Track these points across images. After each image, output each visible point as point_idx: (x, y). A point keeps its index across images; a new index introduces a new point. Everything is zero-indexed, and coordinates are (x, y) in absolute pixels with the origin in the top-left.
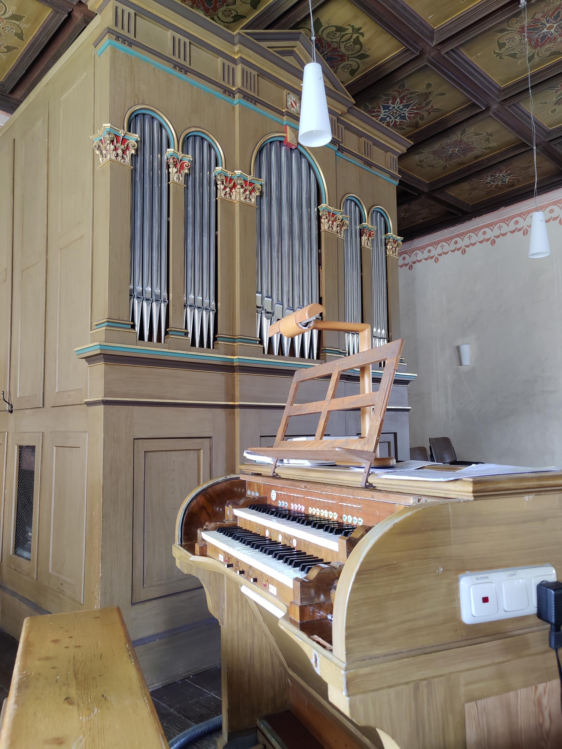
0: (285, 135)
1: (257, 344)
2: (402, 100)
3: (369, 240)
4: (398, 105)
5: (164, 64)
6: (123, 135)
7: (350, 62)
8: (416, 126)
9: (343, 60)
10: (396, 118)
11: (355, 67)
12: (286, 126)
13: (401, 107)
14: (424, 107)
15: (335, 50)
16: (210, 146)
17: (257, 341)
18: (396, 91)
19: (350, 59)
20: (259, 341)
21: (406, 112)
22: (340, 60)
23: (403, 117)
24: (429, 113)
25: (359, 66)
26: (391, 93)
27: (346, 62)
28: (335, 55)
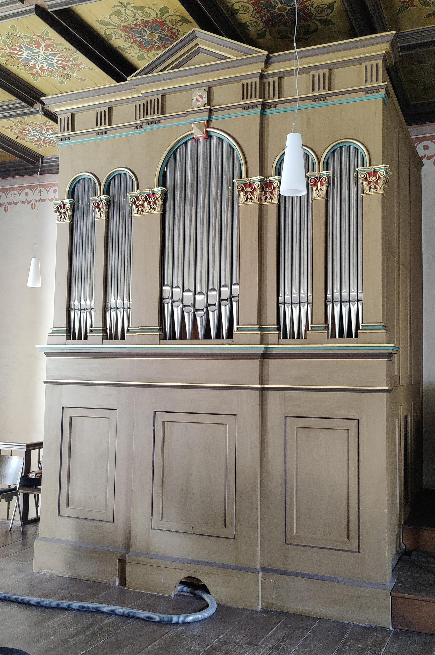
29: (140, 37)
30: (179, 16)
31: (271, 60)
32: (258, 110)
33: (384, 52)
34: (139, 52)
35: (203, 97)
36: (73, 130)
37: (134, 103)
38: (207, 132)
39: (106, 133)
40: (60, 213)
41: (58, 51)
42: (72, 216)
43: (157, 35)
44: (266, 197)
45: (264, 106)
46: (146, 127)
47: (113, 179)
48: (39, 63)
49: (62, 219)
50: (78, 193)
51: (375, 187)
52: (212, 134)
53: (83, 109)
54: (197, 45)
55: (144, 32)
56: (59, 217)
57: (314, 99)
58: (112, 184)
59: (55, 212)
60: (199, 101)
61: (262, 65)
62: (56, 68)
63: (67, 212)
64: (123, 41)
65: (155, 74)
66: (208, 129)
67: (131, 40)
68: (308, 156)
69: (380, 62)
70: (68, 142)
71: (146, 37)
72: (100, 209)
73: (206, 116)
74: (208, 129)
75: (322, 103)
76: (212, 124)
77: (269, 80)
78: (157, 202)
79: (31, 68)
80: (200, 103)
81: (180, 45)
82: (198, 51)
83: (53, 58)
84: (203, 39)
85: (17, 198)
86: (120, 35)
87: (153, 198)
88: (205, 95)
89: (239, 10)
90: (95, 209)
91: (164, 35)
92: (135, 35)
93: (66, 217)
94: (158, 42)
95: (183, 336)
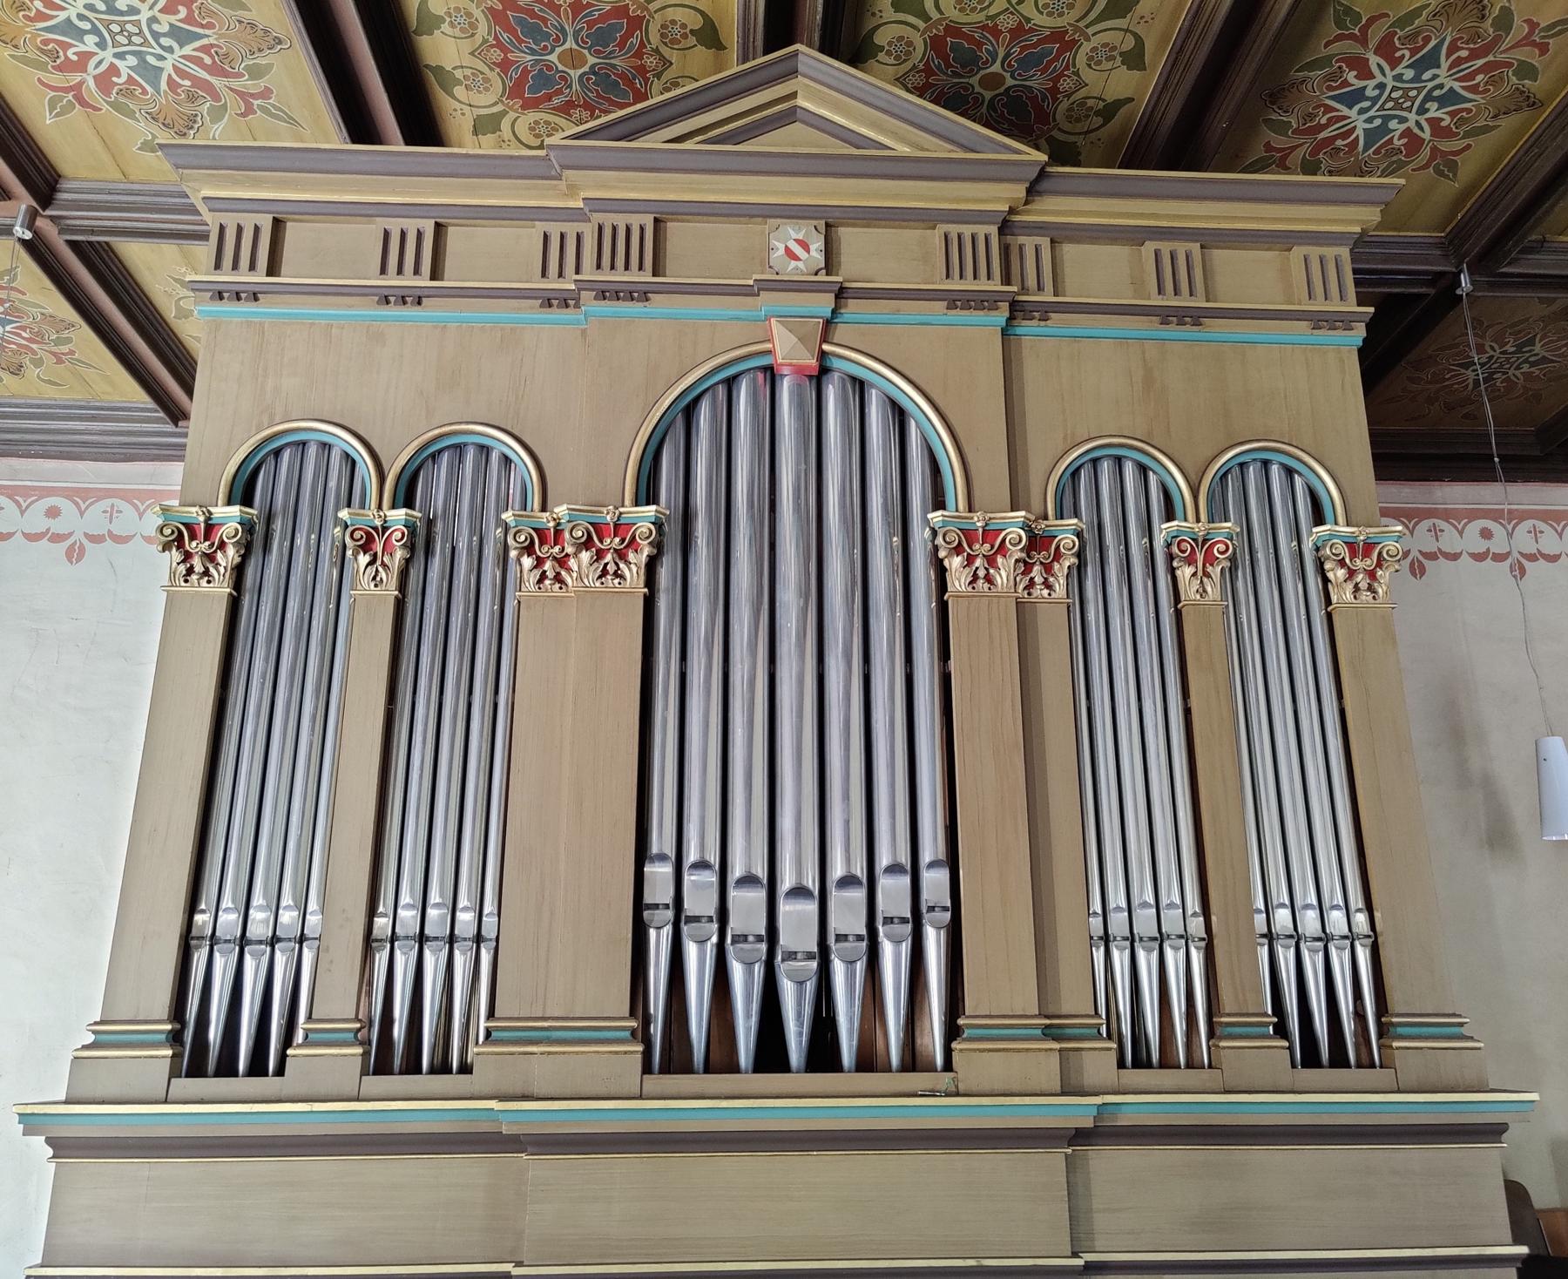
0: (769, 346)
1: (1266, 1037)
2: (1386, 50)
3: (1206, 574)
4: (1383, 74)
5: (350, 307)
6: (202, 519)
7: (1096, 41)
8: (1530, 102)
9: (1072, 45)
10: (1422, 110)
11: (1130, 43)
12: (768, 318)
13: (1409, 74)
14: (1497, 40)
15: (1018, 32)
16: (899, 415)
17: (1266, 1025)
18: (1339, 38)
19: (1090, 31)
20: (1275, 1025)
21: (1443, 76)
22: (1061, 52)
23: (1450, 98)
24: (1544, 48)
25: (1135, 35)
26: (1324, 52)
27: (1086, 47)
28: (1034, 46)
29: (533, 52)
30: (702, 13)
31: (1045, 185)
32: (1000, 317)
33: (1358, 229)
34: (496, 103)
35: (813, 247)
36: (273, 270)
37: (541, 227)
38: (823, 355)
39: (419, 303)
40: (188, 556)
41: (210, 26)
42: (239, 571)
43: (592, 60)
44: (1032, 583)
45: (1018, 310)
46: (592, 306)
47: (271, 459)
48: (108, 55)
49: (194, 577)
50: (276, 486)
51: (1370, 588)
52: (836, 363)
53: (332, 209)
54: (794, 95)
55: (557, 40)
56: (182, 569)
57: (1166, 316)
58: (267, 474)
59: (166, 547)
60: (796, 258)
61: (1019, 191)
62: (164, 86)
63: (219, 555)
64: (466, 46)
65: (653, 141)
66: (826, 347)
67: (496, 55)
68: (354, 462)
69: (1344, 252)
70: (246, 307)
71: (553, 58)
72: (375, 556)
73: (823, 304)
74: (826, 347)
75: (1188, 332)
76: (840, 333)
77: (1022, 239)
78: (631, 556)
79: (66, 67)
80: (800, 264)
81: (721, 91)
82: (791, 116)
83: (175, 46)
84: (829, 87)
85: (1450, 540)
86: (473, 26)
87: (617, 540)
88: (817, 245)
89: (881, 48)
90: (355, 555)
91: (613, 66)
92: (521, 41)
93: (212, 570)
94: (576, 86)
95: (721, 1060)
